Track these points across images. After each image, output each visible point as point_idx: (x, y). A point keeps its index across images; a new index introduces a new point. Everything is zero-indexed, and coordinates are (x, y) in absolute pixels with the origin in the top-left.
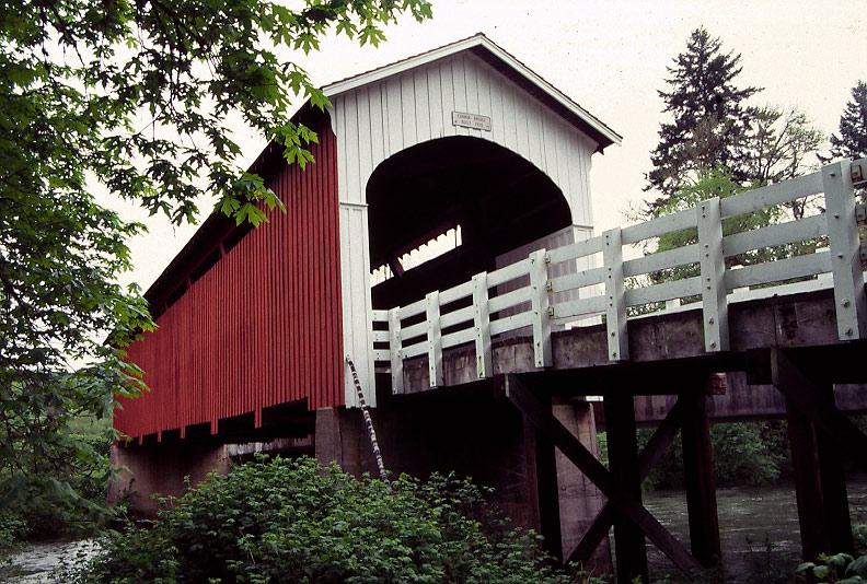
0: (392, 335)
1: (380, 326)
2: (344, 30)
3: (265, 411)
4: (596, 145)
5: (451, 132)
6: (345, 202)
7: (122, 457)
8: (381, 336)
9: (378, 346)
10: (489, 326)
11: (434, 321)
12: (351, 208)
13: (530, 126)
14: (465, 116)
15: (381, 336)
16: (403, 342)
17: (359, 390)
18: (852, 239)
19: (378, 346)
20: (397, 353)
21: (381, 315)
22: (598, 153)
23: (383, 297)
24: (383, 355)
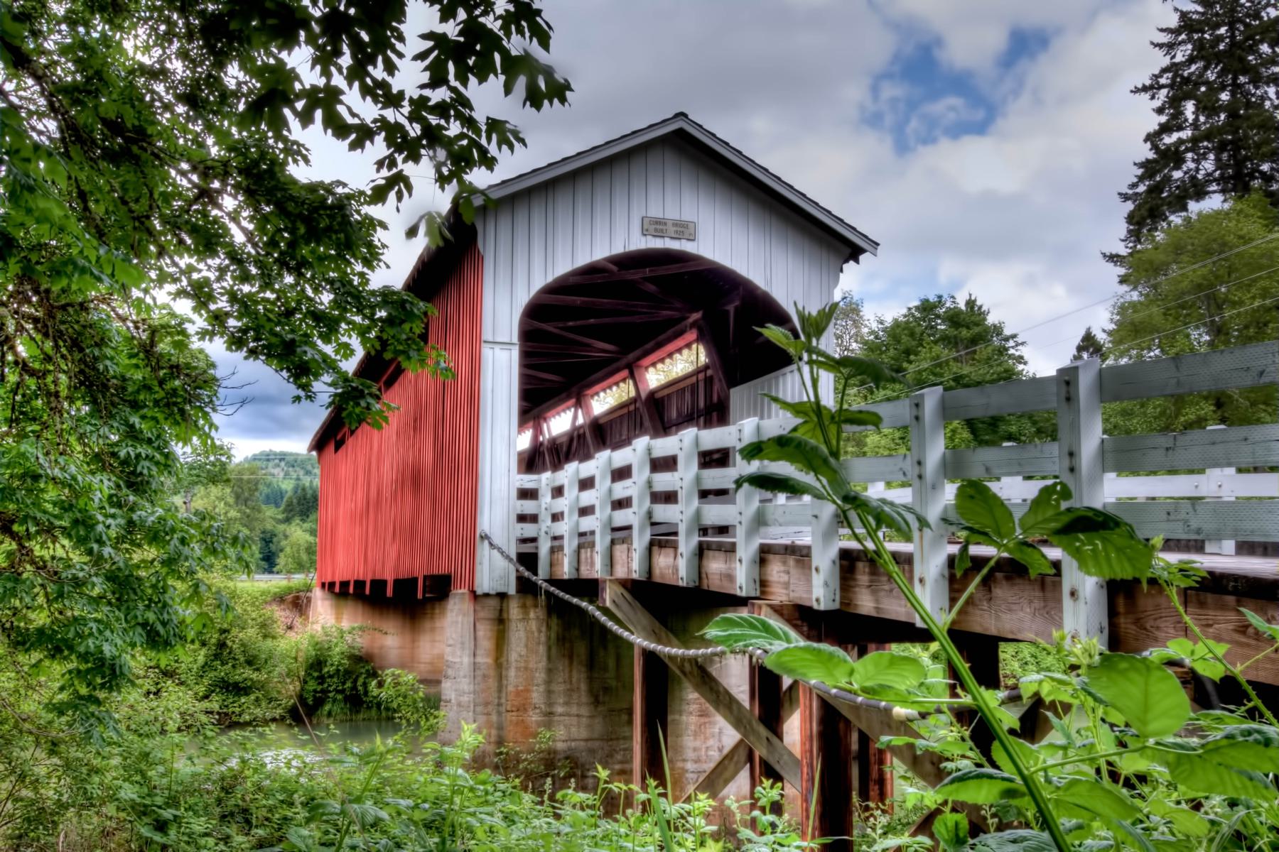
0: (540, 506)
1: (527, 494)
2: (430, 44)
3: (425, 577)
4: (848, 251)
5: (640, 243)
6: (491, 339)
7: (327, 603)
8: (528, 506)
9: (522, 518)
10: (578, 498)
11: (571, 493)
12: (497, 348)
13: (790, 260)
14: (658, 222)
15: (528, 506)
16: (1167, 541)
17: (170, 582)
18: (835, 687)
19: (522, 518)
20: (544, 529)
21: (528, 481)
22: (852, 262)
23: (532, 461)
24: (529, 530)
